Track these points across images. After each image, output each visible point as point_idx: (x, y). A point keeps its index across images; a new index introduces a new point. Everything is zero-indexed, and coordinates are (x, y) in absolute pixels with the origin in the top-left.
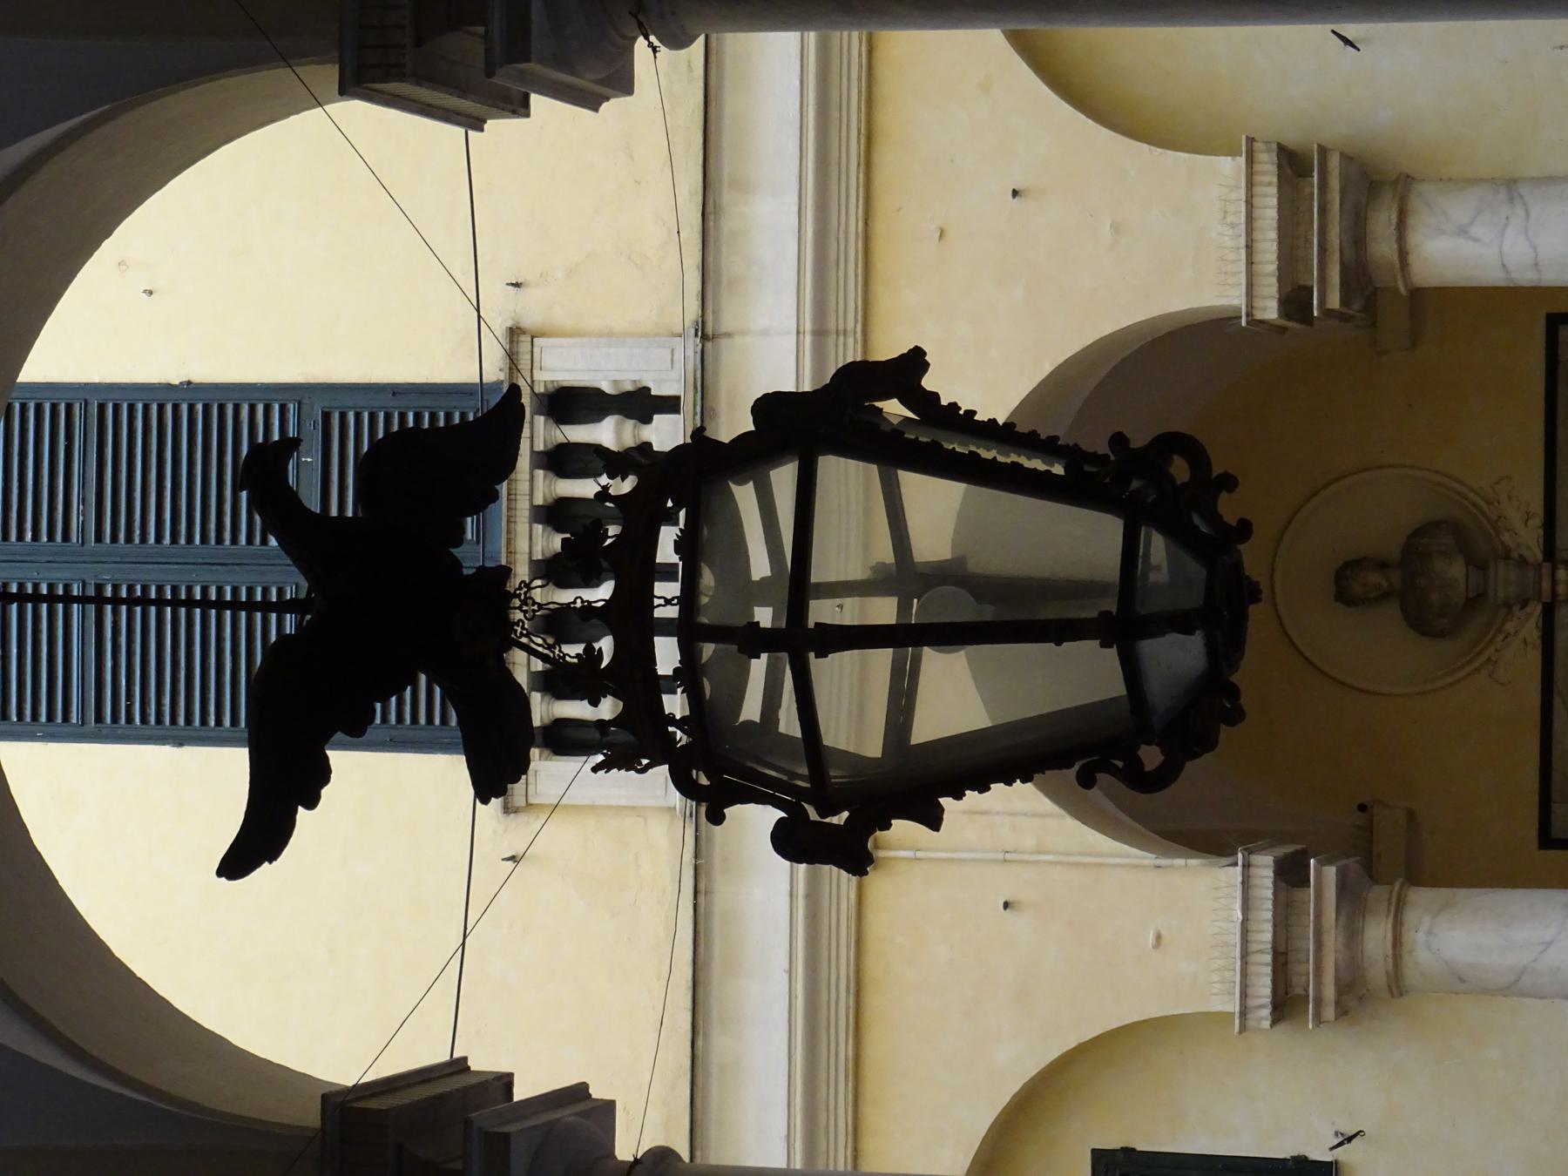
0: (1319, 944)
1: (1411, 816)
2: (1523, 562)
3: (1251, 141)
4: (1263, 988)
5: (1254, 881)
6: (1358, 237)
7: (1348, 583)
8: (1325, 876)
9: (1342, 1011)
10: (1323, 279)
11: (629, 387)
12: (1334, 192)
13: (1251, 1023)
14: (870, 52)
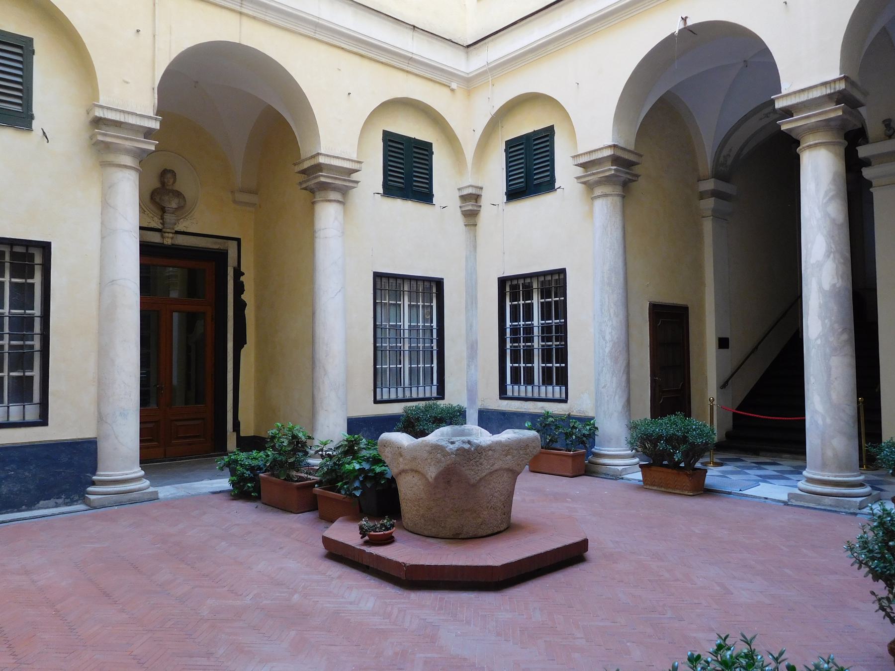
0: (126, 139)
4: (583, 160)
6: (335, 188)
8: (150, 146)
9: (97, 144)
10: (797, 120)
11: (317, 235)
14: (382, 63)
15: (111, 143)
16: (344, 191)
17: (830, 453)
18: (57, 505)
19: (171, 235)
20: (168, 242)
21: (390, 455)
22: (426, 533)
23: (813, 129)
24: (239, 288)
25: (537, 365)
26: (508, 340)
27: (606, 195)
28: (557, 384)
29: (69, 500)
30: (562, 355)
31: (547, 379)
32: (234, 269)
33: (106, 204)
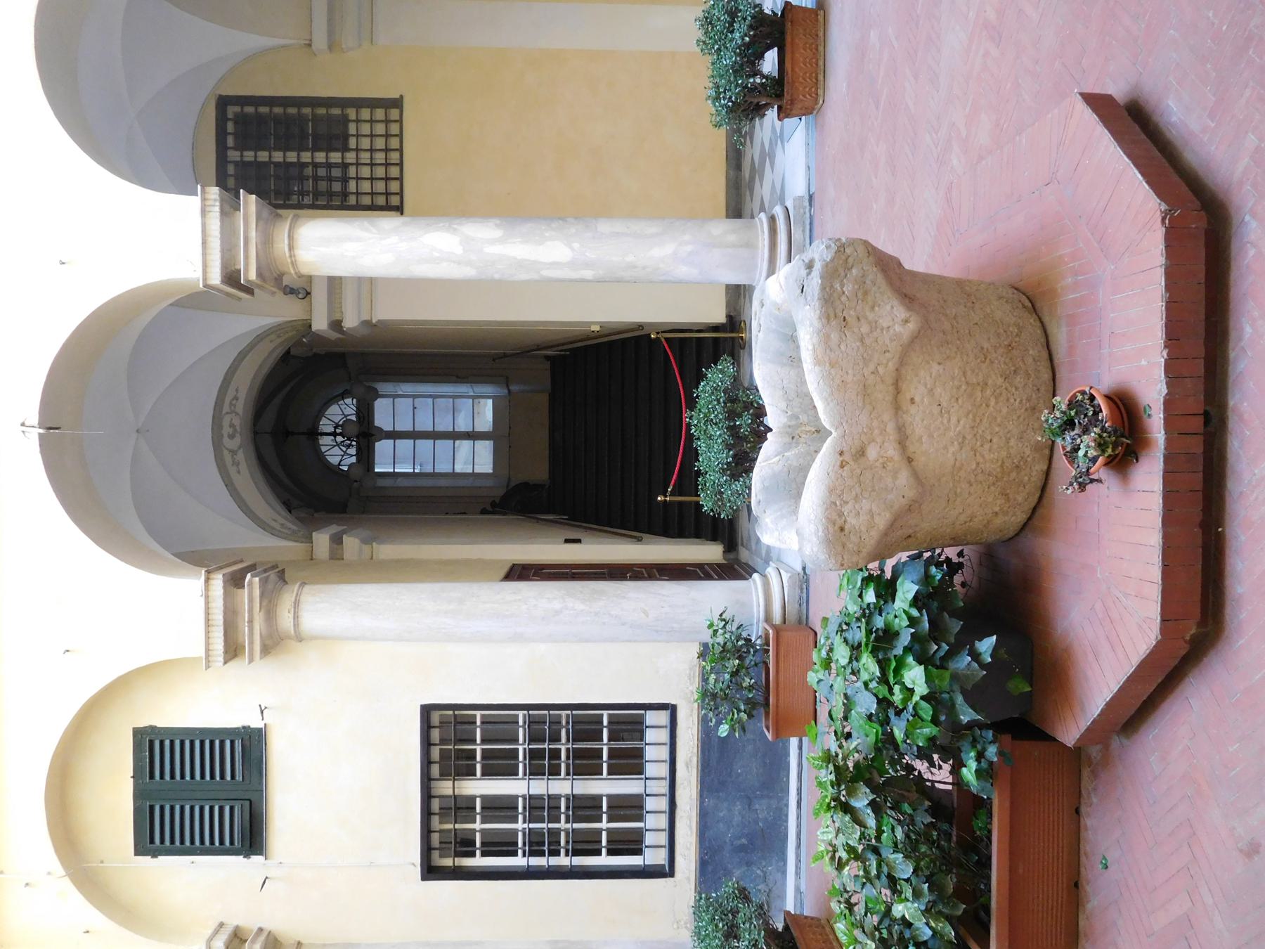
17: (732, 238)
21: (865, 505)
22: (1046, 375)
23: (267, 241)
25: (604, 786)
26: (554, 861)
27: (297, 603)
28: (640, 818)
30: (585, 722)
31: (629, 763)
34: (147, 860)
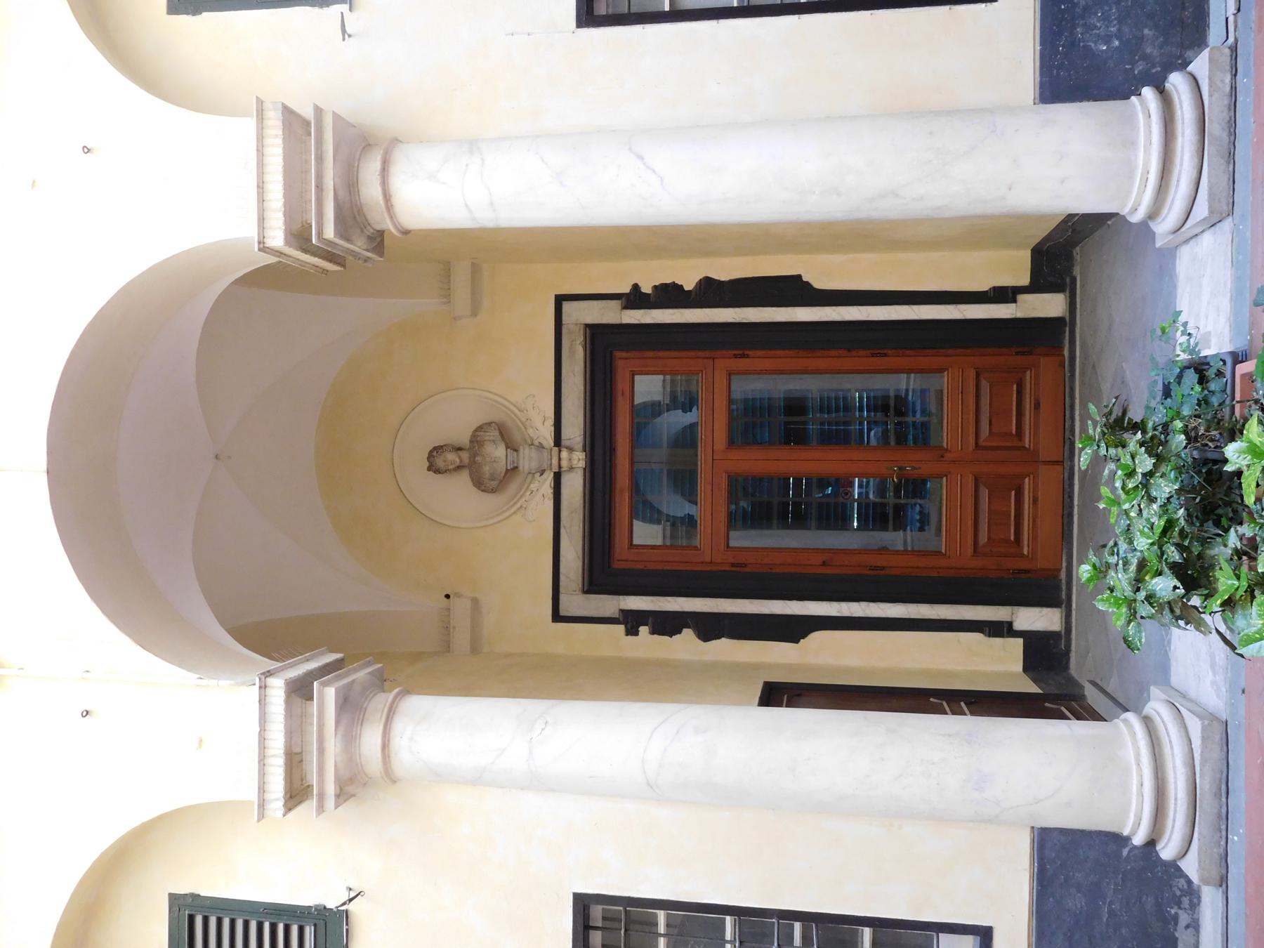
0: (321, 751)
1: (475, 601)
2: (541, 446)
3: (260, 103)
5: (269, 699)
6: (350, 183)
7: (437, 460)
8: (327, 695)
9: (343, 795)
12: (334, 152)
13: (268, 813)
15: (338, 779)
16: (362, 145)
18: (1195, 926)
19: (564, 454)
20: (579, 459)
24: (670, 295)
29: (1186, 901)
32: (626, 307)
33: (478, 780)
34: (184, 20)
